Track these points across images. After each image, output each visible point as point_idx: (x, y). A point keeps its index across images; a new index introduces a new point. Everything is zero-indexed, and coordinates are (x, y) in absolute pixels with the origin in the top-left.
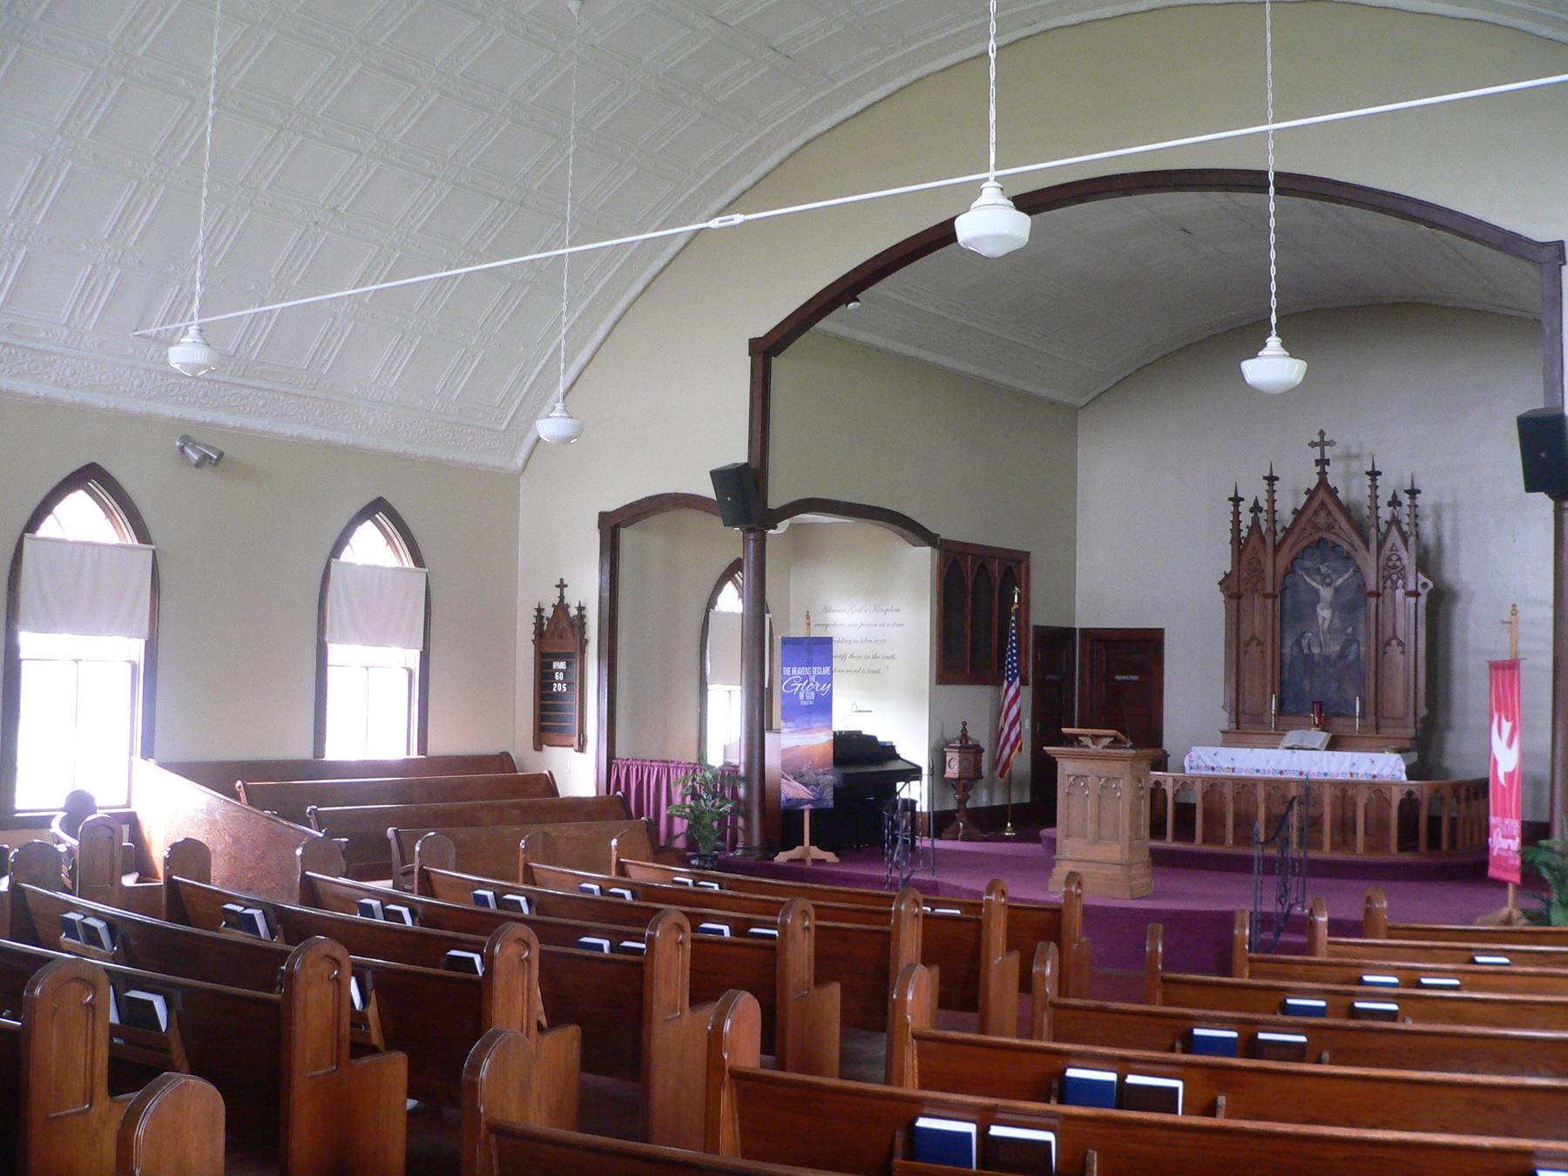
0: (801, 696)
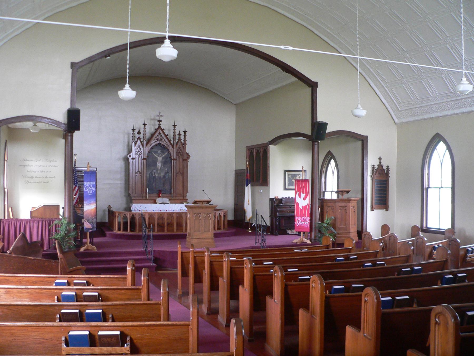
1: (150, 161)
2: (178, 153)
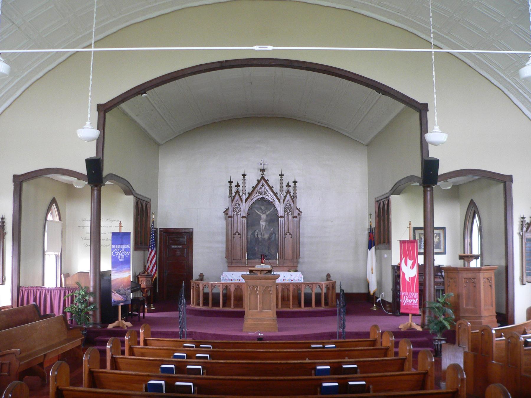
0: (119, 258)
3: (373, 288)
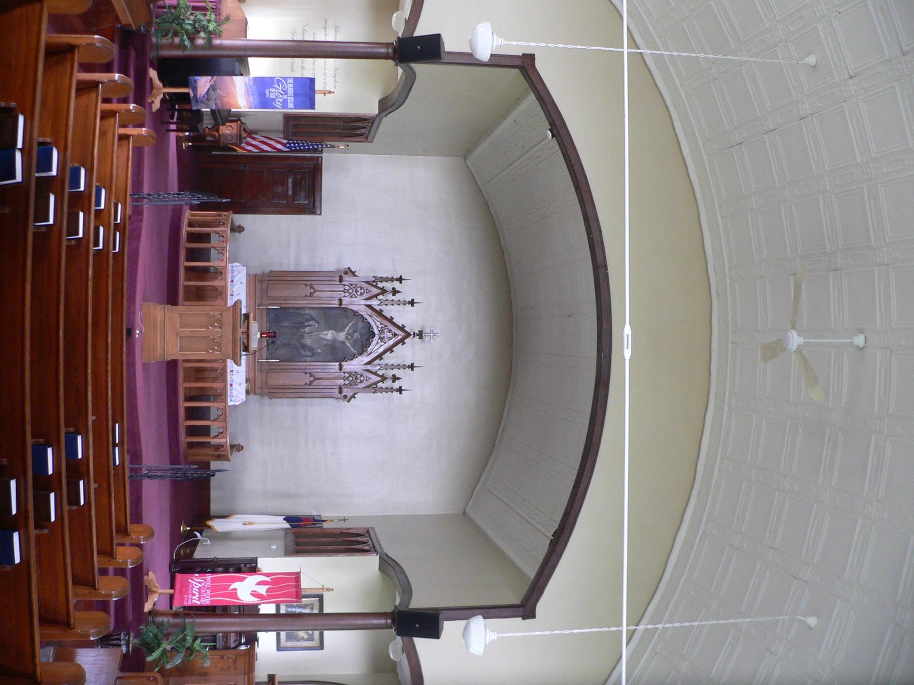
0: (271, 90)
1: (338, 315)
2: (353, 375)
3: (218, 525)
